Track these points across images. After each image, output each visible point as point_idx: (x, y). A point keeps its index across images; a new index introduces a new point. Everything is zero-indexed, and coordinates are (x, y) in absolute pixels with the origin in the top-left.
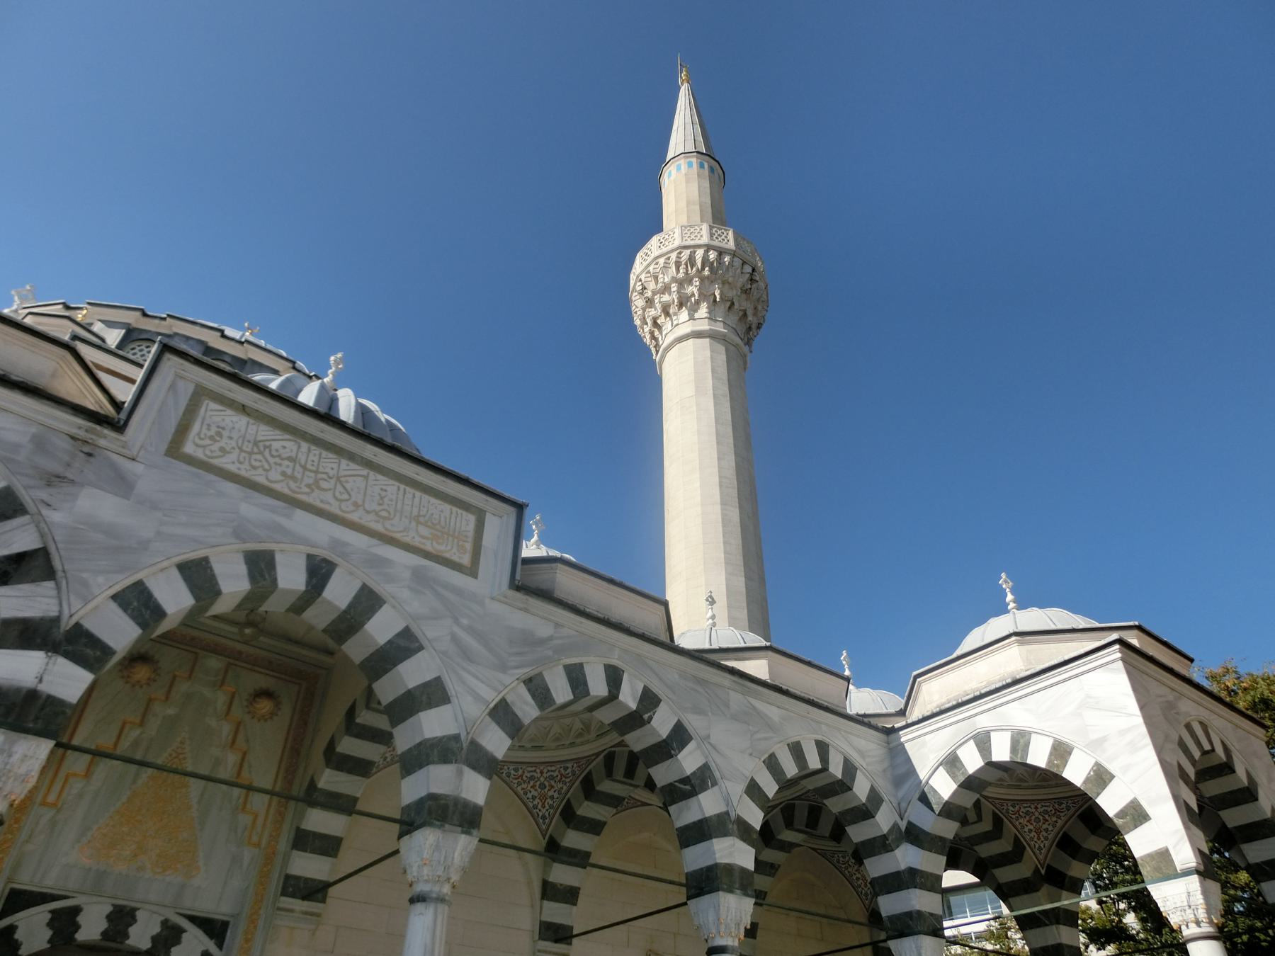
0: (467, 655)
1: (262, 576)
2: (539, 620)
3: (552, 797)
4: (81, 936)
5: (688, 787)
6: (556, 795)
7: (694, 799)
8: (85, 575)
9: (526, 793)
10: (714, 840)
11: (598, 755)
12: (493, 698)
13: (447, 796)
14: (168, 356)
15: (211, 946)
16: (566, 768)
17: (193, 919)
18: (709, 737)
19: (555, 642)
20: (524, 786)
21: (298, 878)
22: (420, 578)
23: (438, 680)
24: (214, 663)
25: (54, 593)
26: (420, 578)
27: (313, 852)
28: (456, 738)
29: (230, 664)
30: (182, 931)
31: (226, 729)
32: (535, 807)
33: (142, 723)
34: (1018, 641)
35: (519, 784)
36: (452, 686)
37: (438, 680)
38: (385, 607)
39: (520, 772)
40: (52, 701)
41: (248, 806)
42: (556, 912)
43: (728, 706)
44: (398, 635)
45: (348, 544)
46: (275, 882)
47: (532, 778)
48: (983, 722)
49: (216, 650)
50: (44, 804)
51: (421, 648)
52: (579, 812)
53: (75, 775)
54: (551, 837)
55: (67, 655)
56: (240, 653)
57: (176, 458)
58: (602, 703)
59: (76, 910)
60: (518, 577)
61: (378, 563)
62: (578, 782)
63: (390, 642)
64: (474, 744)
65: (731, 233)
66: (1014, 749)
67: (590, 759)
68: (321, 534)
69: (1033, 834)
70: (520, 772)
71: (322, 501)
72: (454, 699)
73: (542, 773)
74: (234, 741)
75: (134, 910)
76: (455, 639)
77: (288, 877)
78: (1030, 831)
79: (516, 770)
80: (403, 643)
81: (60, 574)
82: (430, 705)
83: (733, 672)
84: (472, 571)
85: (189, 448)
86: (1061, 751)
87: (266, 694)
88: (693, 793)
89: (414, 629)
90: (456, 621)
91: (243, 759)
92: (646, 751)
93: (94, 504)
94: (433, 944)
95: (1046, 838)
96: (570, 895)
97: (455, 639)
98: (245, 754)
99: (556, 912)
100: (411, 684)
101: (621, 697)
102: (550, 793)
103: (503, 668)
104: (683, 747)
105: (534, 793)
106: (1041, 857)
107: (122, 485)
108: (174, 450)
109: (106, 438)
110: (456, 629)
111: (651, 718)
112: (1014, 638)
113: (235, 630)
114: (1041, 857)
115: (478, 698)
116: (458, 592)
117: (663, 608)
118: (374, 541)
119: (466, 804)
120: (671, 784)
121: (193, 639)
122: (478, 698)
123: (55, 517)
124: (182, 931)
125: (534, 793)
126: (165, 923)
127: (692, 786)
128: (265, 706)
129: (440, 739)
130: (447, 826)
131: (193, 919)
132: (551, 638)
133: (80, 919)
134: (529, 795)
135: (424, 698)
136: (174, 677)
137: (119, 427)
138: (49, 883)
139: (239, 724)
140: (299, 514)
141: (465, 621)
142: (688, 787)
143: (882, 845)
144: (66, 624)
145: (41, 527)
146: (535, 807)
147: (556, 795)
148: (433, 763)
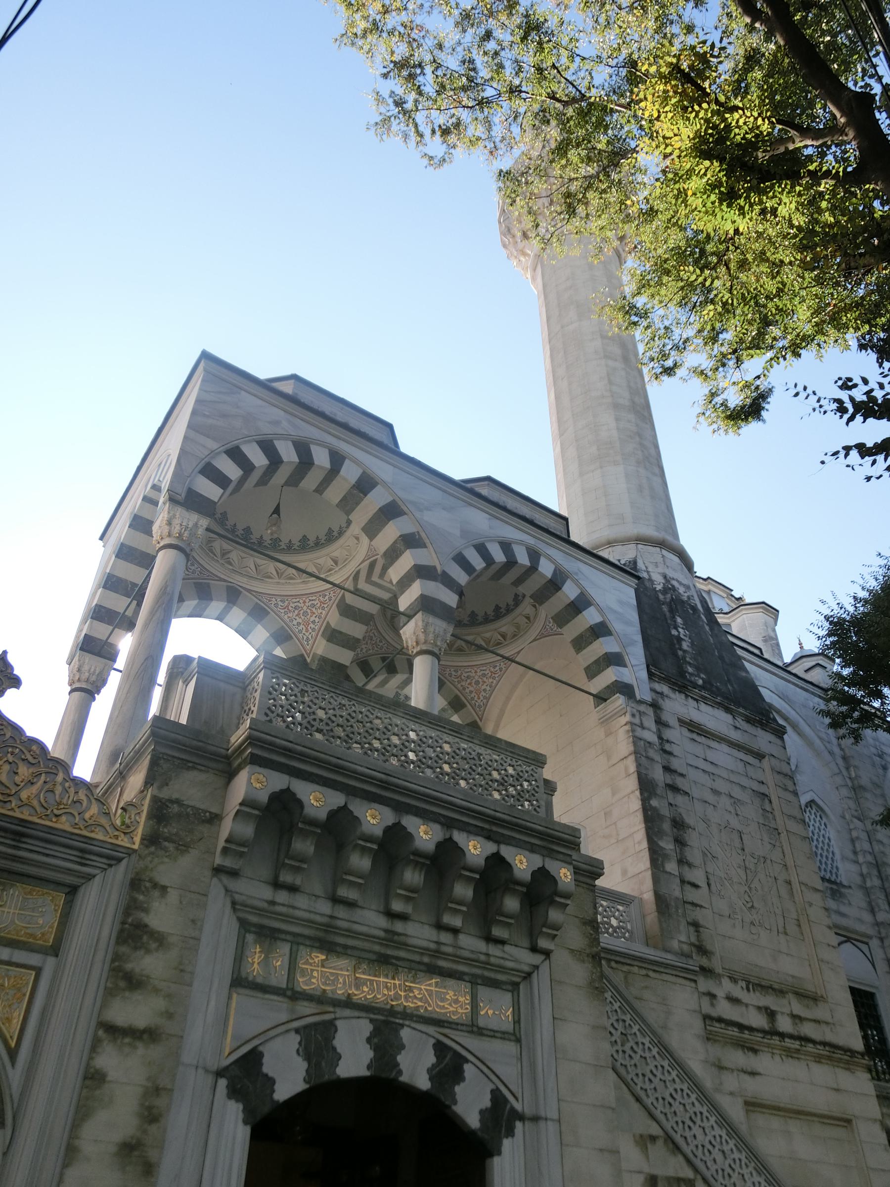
3: (314, 622)
6: (317, 620)
9: (291, 621)
11: (348, 578)
16: (495, 667)
20: (290, 615)
32: (473, 699)
35: (286, 613)
39: (286, 603)
47: (468, 677)
48: (344, 447)
58: (242, 481)
62: (335, 605)
65: (778, 37)
70: (286, 603)
73: (476, 672)
79: (456, 671)
95: (314, 630)
102: (484, 687)
125: (471, 689)
133: (268, 1068)
134: (295, 622)
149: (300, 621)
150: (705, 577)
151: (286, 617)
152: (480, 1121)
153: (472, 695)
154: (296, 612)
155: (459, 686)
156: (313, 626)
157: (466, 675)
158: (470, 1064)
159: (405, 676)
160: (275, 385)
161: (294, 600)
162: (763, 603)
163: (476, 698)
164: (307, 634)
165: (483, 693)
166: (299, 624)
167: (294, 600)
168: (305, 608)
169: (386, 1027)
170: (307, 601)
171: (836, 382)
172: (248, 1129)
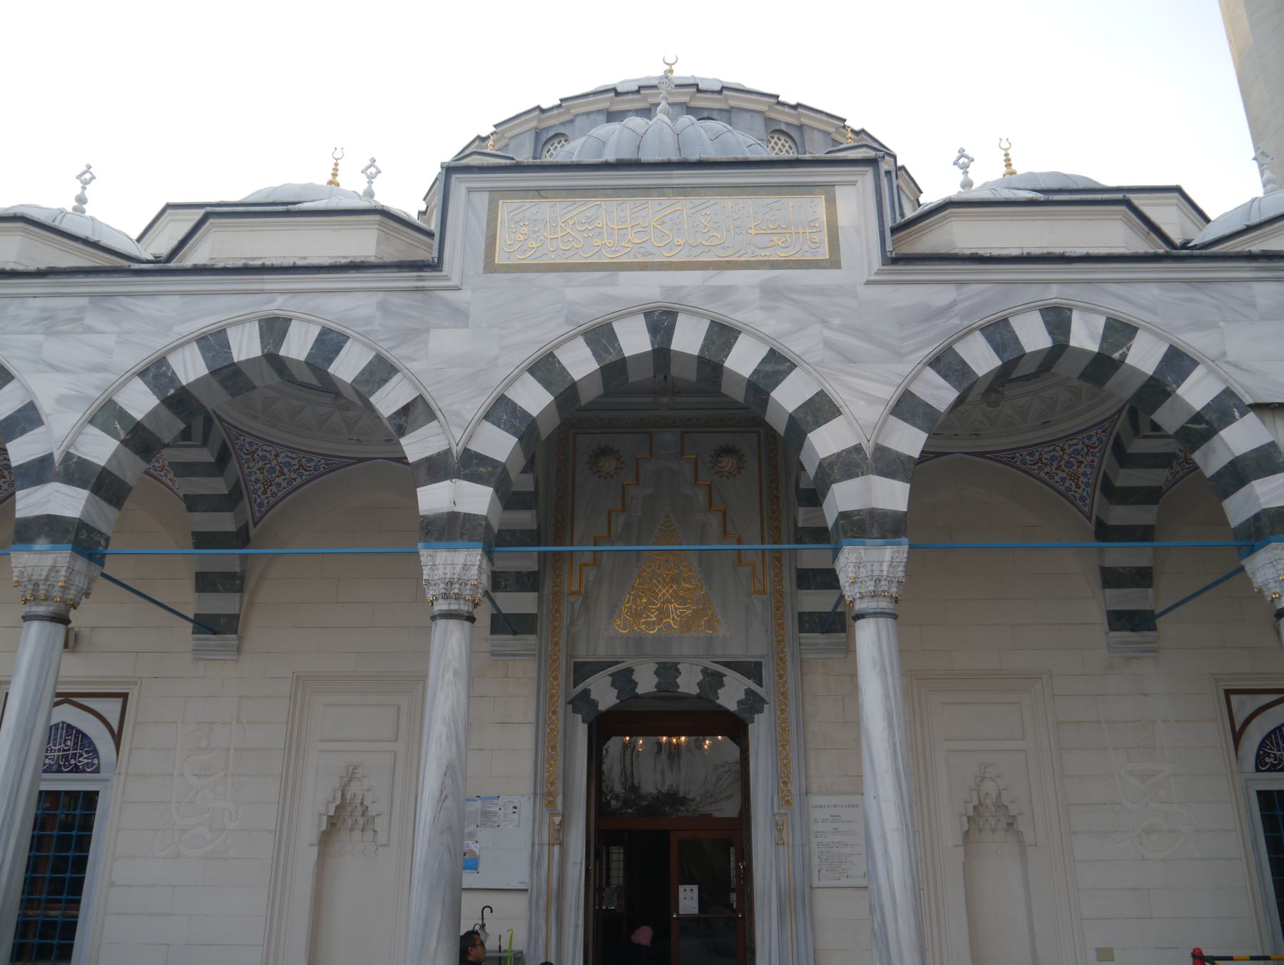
0: (848, 358)
5: (1203, 426)
6: (1089, 471)
8: (455, 407)
10: (1254, 483)
11: (1120, 411)
12: (889, 394)
14: (454, 177)
15: (751, 684)
16: (1090, 438)
18: (1224, 354)
19: (960, 306)
20: (1048, 469)
22: (772, 294)
23: (821, 394)
25: (440, 430)
26: (772, 294)
27: (818, 587)
28: (858, 449)
30: (721, 676)
31: (701, 495)
32: (255, 491)
34: (381, 224)
35: (1040, 469)
36: (839, 395)
37: (821, 394)
39: (1037, 455)
40: (469, 517)
43: (1253, 305)
46: (791, 624)
47: (1053, 459)
50: (572, 593)
53: (586, 565)
54: (1098, 518)
55: (466, 478)
57: (494, 271)
59: (630, 671)
60: (889, 247)
61: (719, 293)
68: (648, 288)
69: (259, 485)
70: (1037, 455)
71: (644, 255)
72: (844, 409)
73: (1063, 449)
76: (827, 344)
81: (438, 413)
83: (1251, 257)
84: (834, 262)
85: (499, 260)
86: (545, 368)
88: (1211, 432)
89: (778, 347)
90: (825, 323)
91: (725, 520)
93: (446, 342)
97: (827, 344)
98: (724, 513)
100: (791, 408)
101: (1073, 343)
102: (1081, 470)
103: (899, 356)
105: (260, 476)
106: (1086, 509)
107: (459, 316)
108: (490, 266)
109: (429, 280)
110: (828, 333)
111: (1124, 356)
112: (377, 217)
114: (1086, 509)
115: (871, 399)
116: (820, 291)
117: (1176, 195)
119: (885, 513)
120: (1183, 428)
122: (871, 399)
123: (415, 366)
124: (721, 676)
125: (260, 476)
126: (705, 671)
127: (1207, 422)
128: (728, 463)
129: (839, 455)
130: (868, 541)
132: (953, 304)
134: (1057, 478)
135: (809, 418)
137: (436, 266)
139: (710, 486)
140: (624, 276)
141: (836, 322)
142: (1203, 426)
143: (1240, 472)
144: (457, 450)
145: (413, 380)
146: (255, 491)
147: (1089, 471)
148: (836, 481)
149: (1064, 475)
150: (793, 102)
152: (639, 944)
153: (1067, 484)
155: (1042, 474)
160: (1237, 728)
165: (1082, 478)
166: (1063, 480)
167: (1047, 449)
168: (1066, 457)
169: (213, 343)
171: (93, 178)
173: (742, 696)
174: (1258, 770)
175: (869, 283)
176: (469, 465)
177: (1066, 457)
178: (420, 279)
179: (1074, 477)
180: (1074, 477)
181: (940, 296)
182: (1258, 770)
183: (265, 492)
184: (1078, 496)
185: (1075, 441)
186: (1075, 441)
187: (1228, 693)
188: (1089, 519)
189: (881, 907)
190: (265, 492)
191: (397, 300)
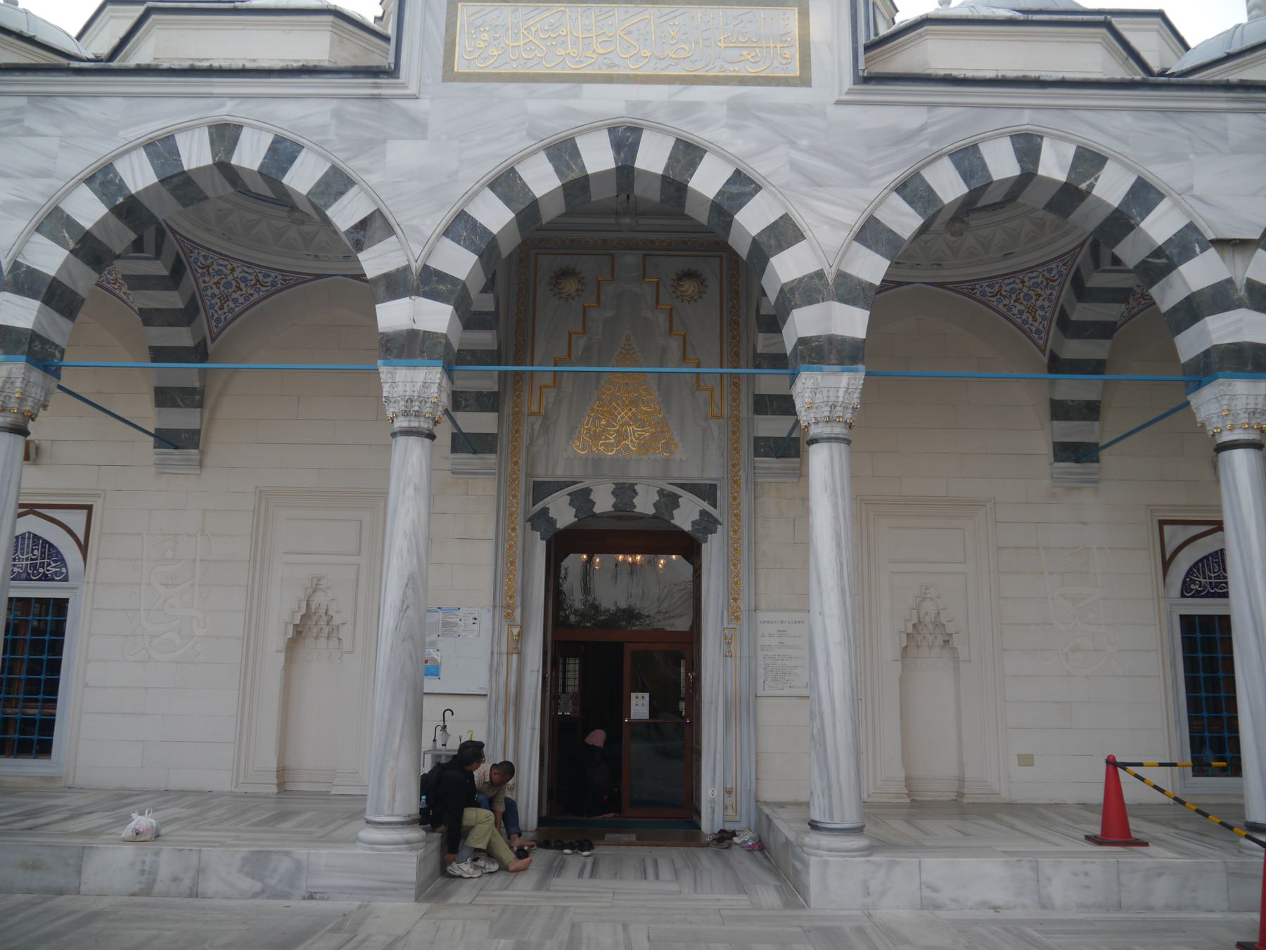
0: (814, 181)
1: (570, 168)
2: (900, 115)
3: (1042, 308)
4: (598, 509)
5: (1163, 261)
6: (1046, 304)
7: (1174, 272)
11: (1082, 244)
12: (854, 219)
13: (819, 337)
16: (1050, 271)
17: (682, 486)
19: (930, 130)
21: (766, 439)
23: (786, 218)
24: (630, 259)
26: (739, 111)
27: (773, 413)
28: (820, 274)
29: (645, 255)
30: (678, 497)
31: (662, 319)
32: (212, 307)
33: (585, 331)
35: (999, 301)
36: (803, 219)
37: (786, 218)
38: (707, 156)
40: (428, 335)
41: (702, 384)
42: (1075, 431)
44: (728, 182)
45: (649, 102)
46: (746, 447)
47: (1012, 291)
49: (629, 246)
51: (758, 188)
52: (1074, 318)
53: (546, 386)
55: (426, 295)
56: (652, 242)
59: (588, 491)
60: (861, 66)
61: (687, 109)
63: (720, 193)
64: (842, 276)
66: (966, 176)
67: (1074, 252)
68: (613, 102)
70: (997, 287)
71: (609, 66)
72: (807, 234)
73: (1022, 282)
74: (671, 330)
75: (633, 485)
76: (794, 166)
77: (757, 439)
78: (1021, 312)
80: (734, 189)
81: (397, 229)
82: (781, 248)
85: (459, 67)
87: (689, 275)
88: (1171, 267)
90: (792, 144)
92: (1101, 229)
93: (403, 154)
94: (833, 480)
95: (1044, 318)
96: (1090, 410)
97: (794, 166)
99: (1075, 431)
101: (1042, 171)
102: (1039, 303)
104: (1148, 211)
107: (417, 127)
108: (449, 75)
109: (386, 87)
110: (795, 155)
111: (1092, 186)
113: (612, 221)
115: (835, 224)
116: (789, 110)
117: (1158, 20)
118: (677, 87)
119: (843, 341)
120: (1144, 262)
121: (572, 241)
122: (835, 224)
124: (678, 497)
126: (661, 492)
127: (1167, 257)
128: (689, 287)
129: (800, 280)
130: (825, 367)
131: (682, 486)
132: (923, 128)
134: (1015, 311)
135: (773, 242)
136: (599, 282)
137: (391, 72)
138: (560, 473)
139: (671, 310)
140: (587, 88)
141: (804, 143)
142: (1163, 261)
144: (416, 267)
145: (371, 193)
146: (212, 307)
148: (797, 306)
149: (1022, 307)
151: (1000, 306)
154: (1014, 296)
155: (1000, 306)
156: (1042, 313)
157: (1007, 288)
158: (688, 568)
159: (278, 146)
161: (1007, 281)
162: (1160, 14)
163: (1030, 321)
164: (1036, 324)
165: (1040, 312)
167: (1007, 281)
169: (161, 149)
170: (1026, 279)
172: (544, 543)
173: (696, 517)
174: (1183, 596)
175: (839, 103)
176: (429, 283)
177: (1025, 290)
178: (376, 86)
179: (1032, 310)
180: (1032, 310)
181: (911, 119)
182: (1183, 596)
183: (221, 308)
184: (1034, 329)
185: (1035, 274)
186: (1035, 274)
187: (1162, 523)
188: (1043, 352)
189: (821, 714)
190: (221, 308)
191: (353, 108)
